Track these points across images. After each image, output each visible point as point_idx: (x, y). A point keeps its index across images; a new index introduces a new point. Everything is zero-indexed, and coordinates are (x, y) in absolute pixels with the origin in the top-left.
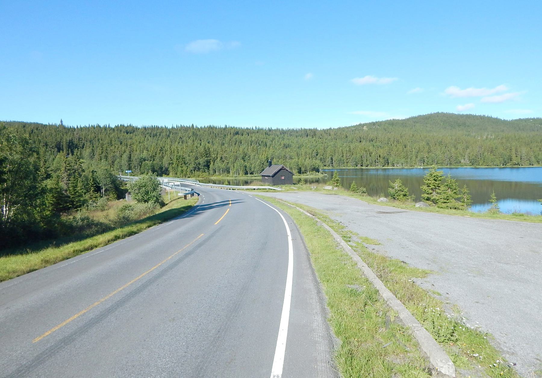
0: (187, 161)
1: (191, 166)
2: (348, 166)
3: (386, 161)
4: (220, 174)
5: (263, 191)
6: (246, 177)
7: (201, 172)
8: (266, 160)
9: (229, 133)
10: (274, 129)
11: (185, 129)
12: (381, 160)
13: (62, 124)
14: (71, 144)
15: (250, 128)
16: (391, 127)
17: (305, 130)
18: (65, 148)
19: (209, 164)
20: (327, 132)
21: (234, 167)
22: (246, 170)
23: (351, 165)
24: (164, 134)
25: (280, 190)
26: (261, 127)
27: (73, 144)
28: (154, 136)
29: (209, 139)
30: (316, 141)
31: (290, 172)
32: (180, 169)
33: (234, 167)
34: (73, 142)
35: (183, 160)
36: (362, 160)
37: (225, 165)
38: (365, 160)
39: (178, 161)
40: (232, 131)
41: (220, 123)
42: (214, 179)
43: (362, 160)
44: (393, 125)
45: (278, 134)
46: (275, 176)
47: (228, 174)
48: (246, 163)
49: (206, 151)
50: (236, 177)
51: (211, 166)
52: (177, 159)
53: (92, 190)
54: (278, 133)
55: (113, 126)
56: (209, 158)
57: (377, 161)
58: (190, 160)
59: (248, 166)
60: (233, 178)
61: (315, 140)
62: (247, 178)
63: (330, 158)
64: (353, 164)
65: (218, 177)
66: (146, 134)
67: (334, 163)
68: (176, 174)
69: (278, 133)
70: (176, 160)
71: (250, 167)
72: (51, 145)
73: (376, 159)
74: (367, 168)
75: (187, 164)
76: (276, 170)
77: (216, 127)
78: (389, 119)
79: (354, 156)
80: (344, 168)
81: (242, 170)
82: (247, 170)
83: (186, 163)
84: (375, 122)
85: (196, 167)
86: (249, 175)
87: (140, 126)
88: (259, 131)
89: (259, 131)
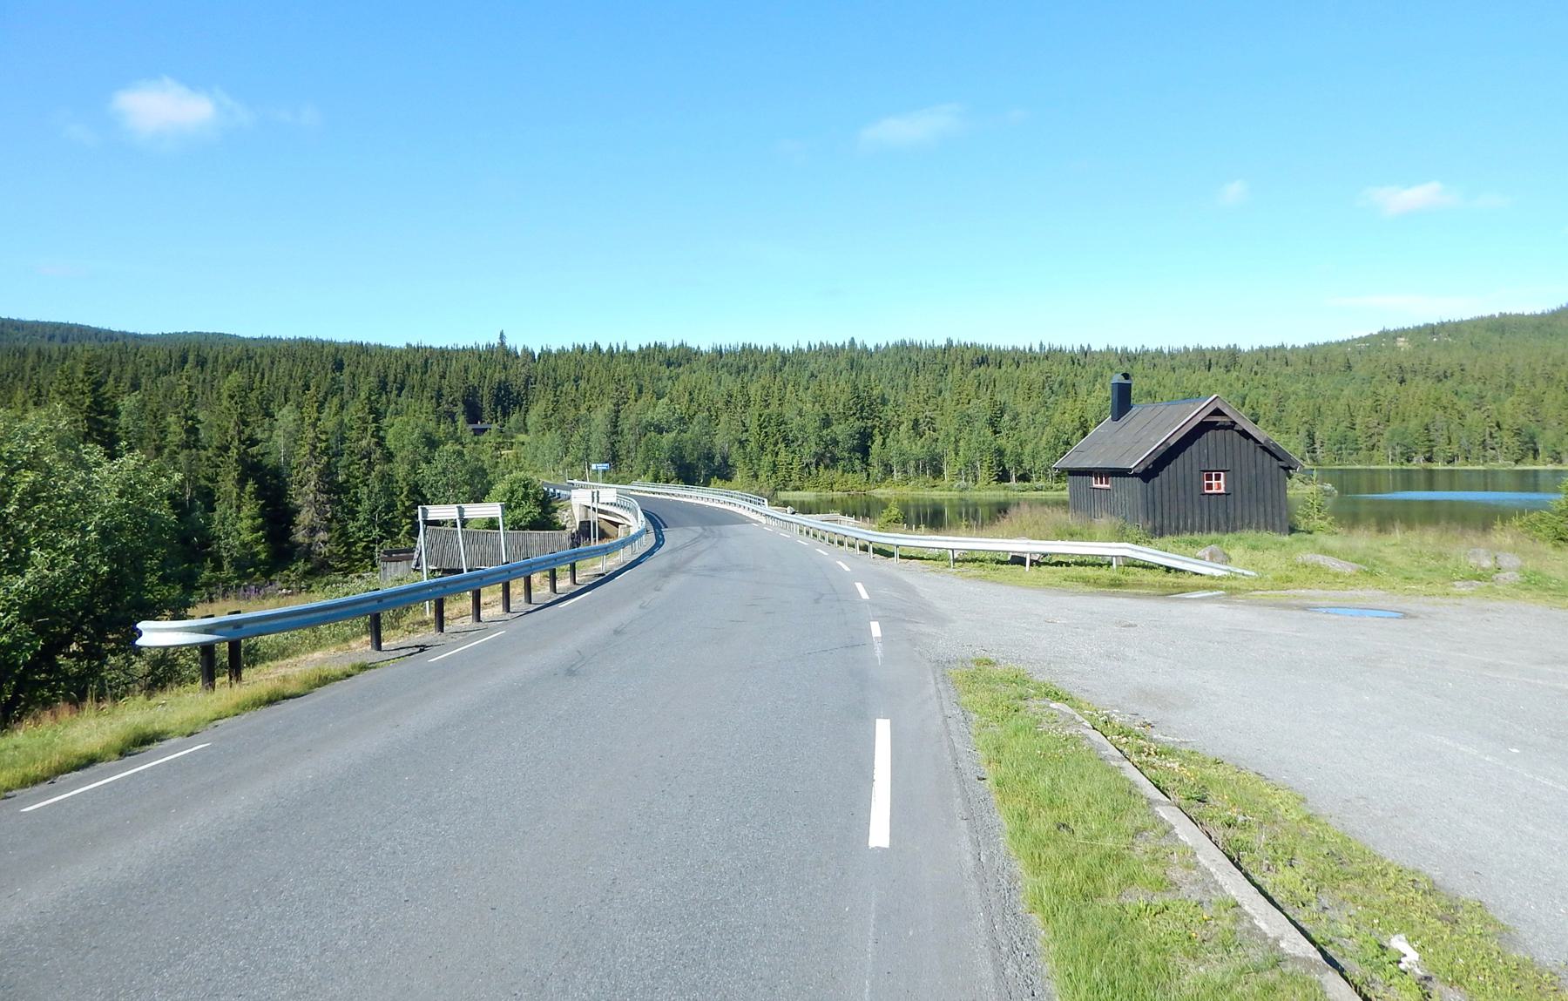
1: (807, 451)
2: (1375, 459)
3: (1526, 443)
4: (906, 480)
5: (1086, 581)
6: (1002, 493)
7: (840, 472)
8: (1078, 430)
9: (959, 362)
10: (1098, 350)
11: (830, 353)
12: (1506, 439)
13: (502, 344)
14: (503, 392)
15: (1025, 348)
16: (1496, 338)
17: (1200, 352)
18: (488, 405)
19: (869, 444)
20: (1267, 356)
21: (957, 454)
22: (1000, 464)
23: (1388, 457)
24: (767, 365)
25: (1217, 573)
26: (1056, 345)
27: (508, 393)
28: (738, 373)
29: (897, 377)
30: (1241, 382)
31: (1265, 449)
33: (957, 454)
36: (1430, 441)
37: (923, 447)
38: (1443, 441)
39: (763, 434)
40: (968, 356)
41: (931, 331)
42: (886, 496)
43: (1431, 438)
44: (1503, 331)
45: (1111, 361)
46: (1164, 474)
47: (935, 478)
48: (1004, 442)
49: (858, 397)
50: (966, 489)
51: (875, 448)
52: (760, 426)
53: (406, 528)
54: (1114, 361)
55: (633, 347)
56: (870, 423)
57: (1489, 441)
58: (802, 429)
59: (1008, 452)
60: (955, 495)
61: (1238, 379)
62: (1006, 495)
63: (1303, 432)
64: (1394, 455)
65: (899, 488)
66: (719, 366)
67: (1319, 451)
68: (756, 476)
69: (1114, 361)
71: (1018, 455)
72: (451, 396)
73: (1487, 437)
74: (1450, 467)
75: (793, 442)
76: (1169, 433)
77: (921, 344)
78: (1486, 313)
79: (1395, 424)
80: (1358, 467)
81: (985, 464)
82: (1007, 467)
84: (1435, 324)
85: (823, 455)
86: (1013, 482)
87: (706, 347)
88: (1051, 355)
89: (1051, 355)
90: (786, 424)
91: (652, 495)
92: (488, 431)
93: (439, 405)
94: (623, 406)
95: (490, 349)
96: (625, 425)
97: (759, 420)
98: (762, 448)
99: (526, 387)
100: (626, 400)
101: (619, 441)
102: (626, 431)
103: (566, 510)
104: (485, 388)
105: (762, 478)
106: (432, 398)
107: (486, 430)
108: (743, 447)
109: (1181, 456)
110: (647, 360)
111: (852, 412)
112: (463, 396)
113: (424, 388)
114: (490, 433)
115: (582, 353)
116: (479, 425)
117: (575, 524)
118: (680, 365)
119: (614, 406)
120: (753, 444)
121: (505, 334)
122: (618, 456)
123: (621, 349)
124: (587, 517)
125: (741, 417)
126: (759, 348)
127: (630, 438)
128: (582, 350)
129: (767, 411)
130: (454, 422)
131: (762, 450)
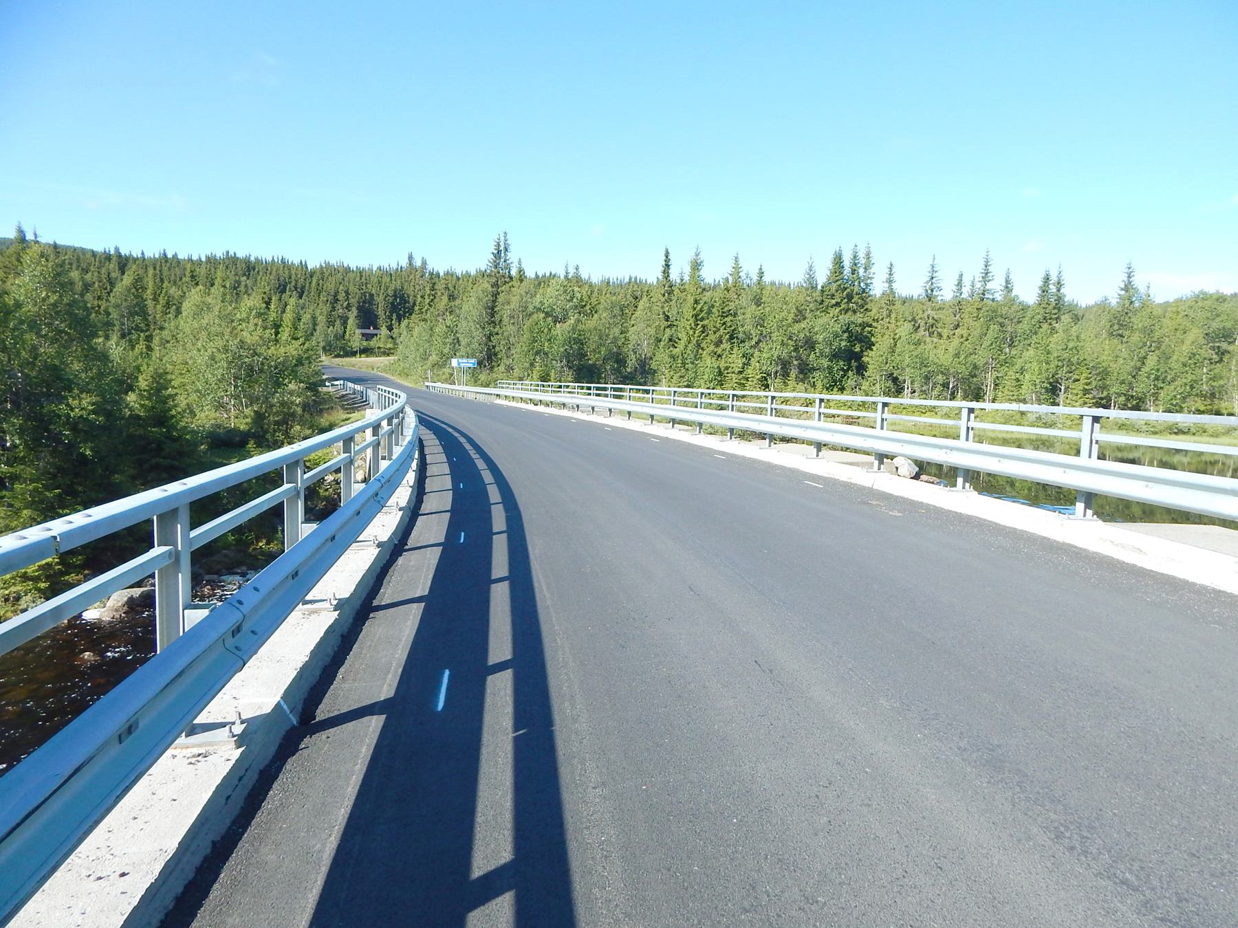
27: (404, 300)
32: (708, 362)
52: (696, 316)
70: (692, 321)
75: (743, 342)
83: (741, 335)
91: (531, 407)
93: (334, 309)
94: (503, 288)
96: (504, 312)
97: (695, 309)
100: (507, 280)
101: (497, 334)
102: (506, 320)
106: (327, 301)
109: (428, 431)
111: (834, 302)
112: (359, 302)
113: (320, 292)
114: (380, 338)
116: (372, 331)
119: (492, 286)
122: (496, 355)
125: (663, 307)
127: (510, 329)
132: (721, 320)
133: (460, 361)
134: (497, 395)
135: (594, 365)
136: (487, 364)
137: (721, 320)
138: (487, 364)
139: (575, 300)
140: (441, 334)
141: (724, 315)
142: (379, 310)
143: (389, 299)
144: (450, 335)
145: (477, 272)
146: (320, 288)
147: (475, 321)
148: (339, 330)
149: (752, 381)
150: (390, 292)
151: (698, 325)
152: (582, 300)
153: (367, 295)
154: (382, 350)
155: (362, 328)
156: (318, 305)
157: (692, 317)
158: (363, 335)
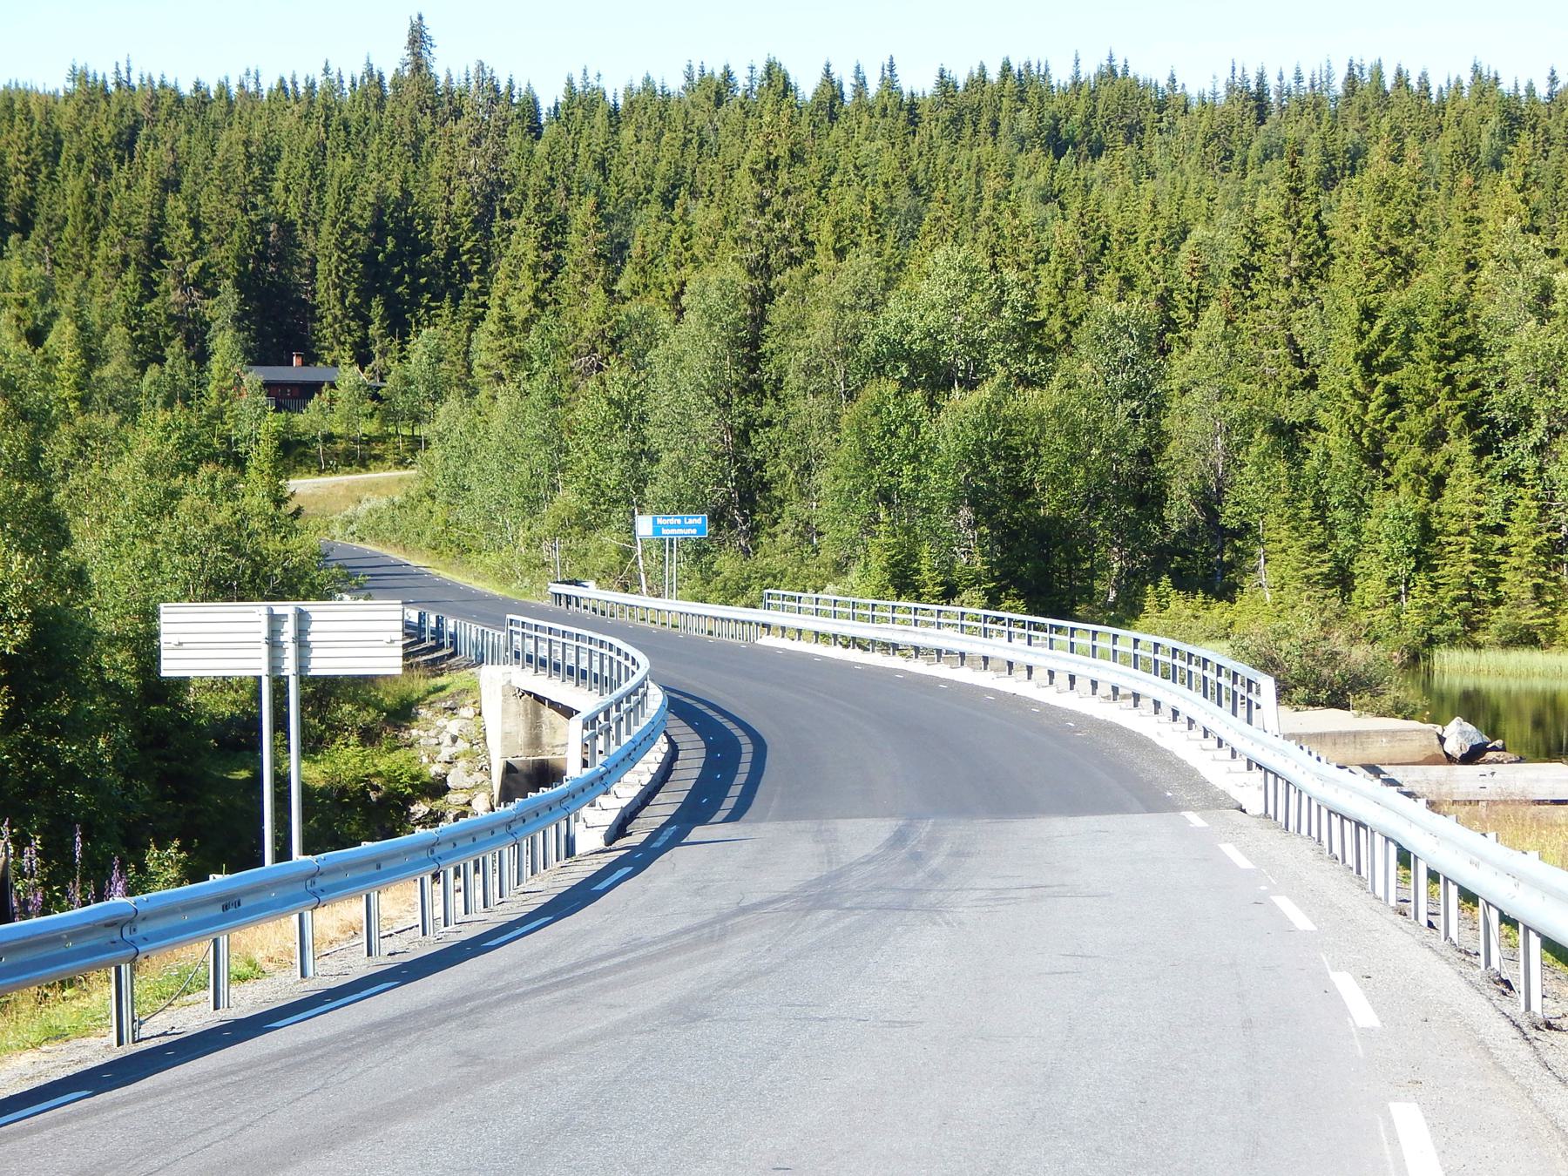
0: (1519, 386)
13: (419, 66)
14: (390, 244)
27: (412, 245)
34: (410, 220)
35: (1449, 380)
39: (1378, 396)
52: (1367, 360)
55: (918, 82)
66: (1254, 152)
68: (1342, 579)
75: (1513, 431)
90: (1479, 352)
91: (836, 652)
92: (326, 394)
93: (149, 289)
95: (373, 90)
98: (1374, 457)
99: (482, 223)
101: (768, 423)
102: (793, 380)
103: (452, 710)
104: (325, 228)
105: (1370, 588)
106: (125, 261)
107: (315, 387)
108: (1289, 454)
110: (968, 131)
112: (242, 260)
114: (332, 400)
115: (719, 103)
116: (296, 371)
117: (489, 774)
118: (1097, 151)
120: (1333, 440)
121: (432, 29)
122: (765, 486)
123: (873, 87)
124: (535, 741)
125: (1285, 323)
126: (1414, 83)
127: (807, 408)
128: (719, 91)
129: (1395, 299)
130: (202, 357)
131: (1375, 462)
132: (1439, 370)
133: (660, 521)
134: (764, 625)
135: (1056, 520)
136: (739, 520)
137: (1439, 370)
138: (739, 520)
139: (1006, 312)
140: (591, 427)
141: (1450, 353)
142: (321, 285)
143: (356, 242)
144: (622, 428)
145: (689, 78)
146: (96, 210)
147: (701, 385)
148: (182, 375)
149: (1521, 555)
150: (361, 214)
151: (1376, 383)
152: (1030, 308)
153: (272, 227)
154: (340, 446)
155: (264, 363)
156: (89, 274)
157: (1356, 360)
158: (270, 387)
